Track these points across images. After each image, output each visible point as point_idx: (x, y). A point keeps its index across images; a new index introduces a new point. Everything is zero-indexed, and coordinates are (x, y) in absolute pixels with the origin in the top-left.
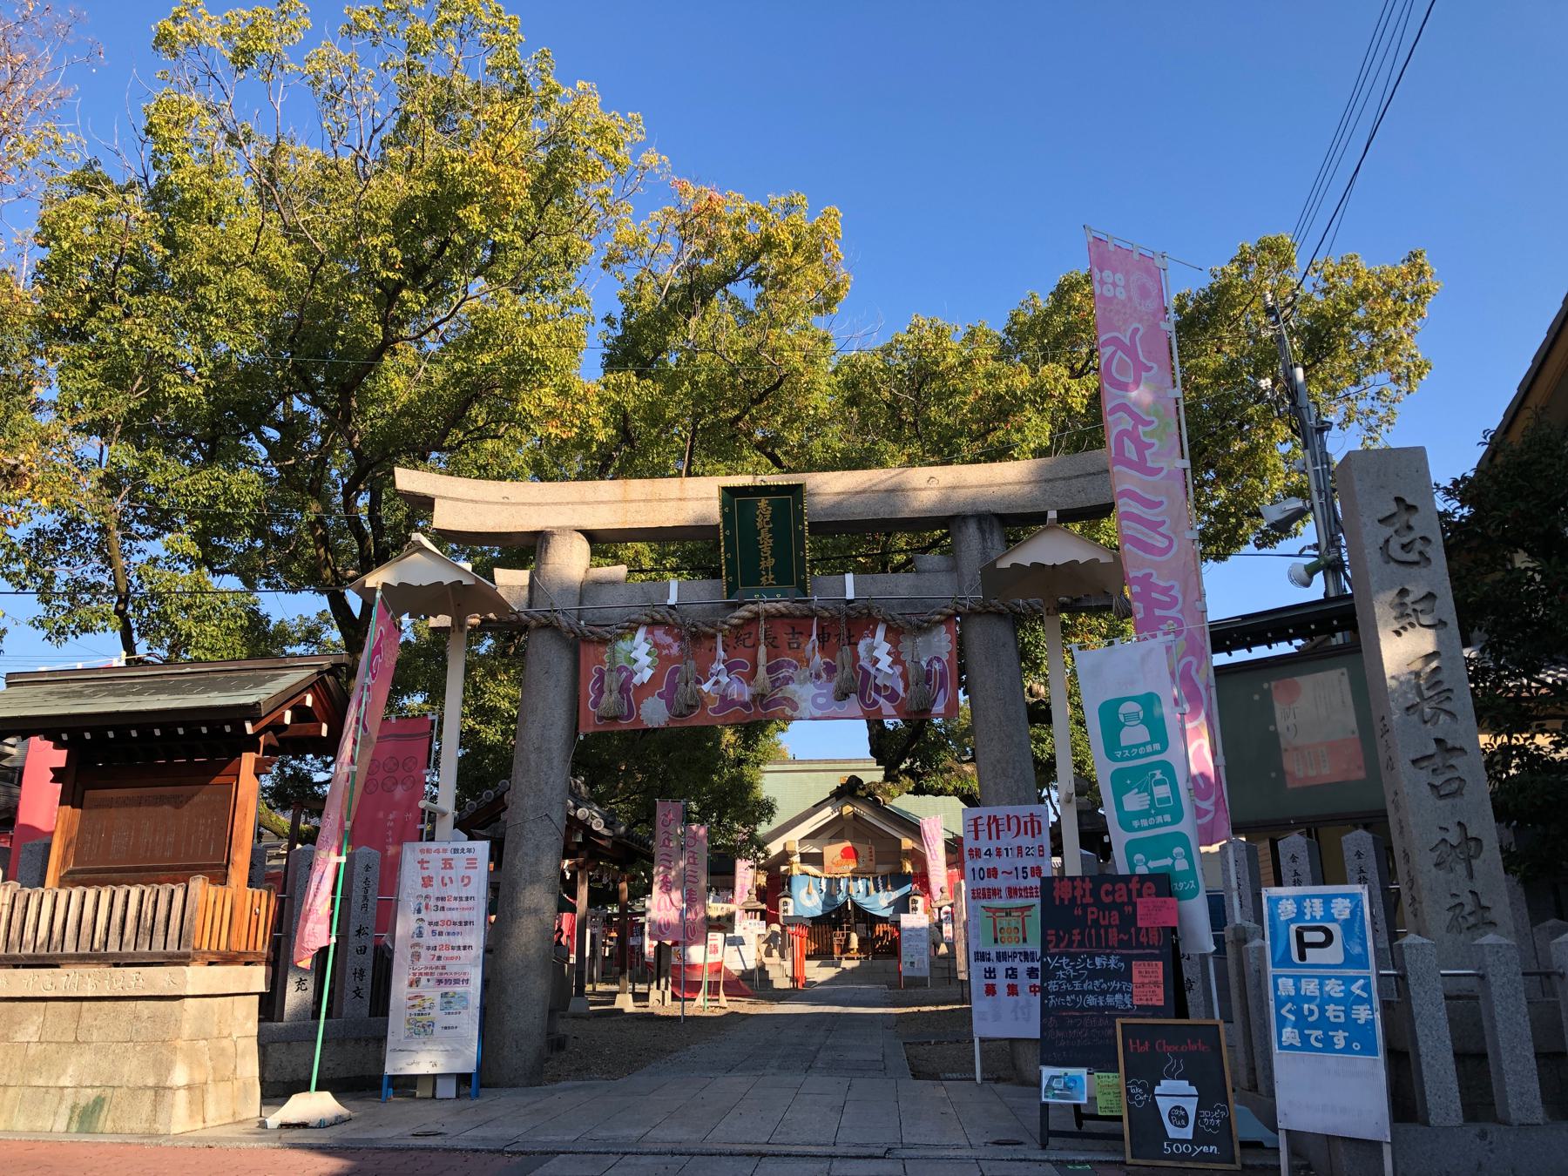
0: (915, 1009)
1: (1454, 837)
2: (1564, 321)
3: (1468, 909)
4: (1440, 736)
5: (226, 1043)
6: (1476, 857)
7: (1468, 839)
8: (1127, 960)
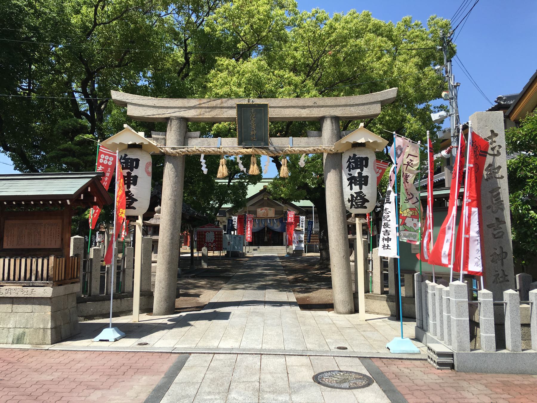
0: (458, 164)
1: (498, 252)
2: (536, 78)
3: (500, 275)
4: (497, 217)
5: (67, 311)
6: (505, 258)
7: (503, 252)
8: (216, 221)
